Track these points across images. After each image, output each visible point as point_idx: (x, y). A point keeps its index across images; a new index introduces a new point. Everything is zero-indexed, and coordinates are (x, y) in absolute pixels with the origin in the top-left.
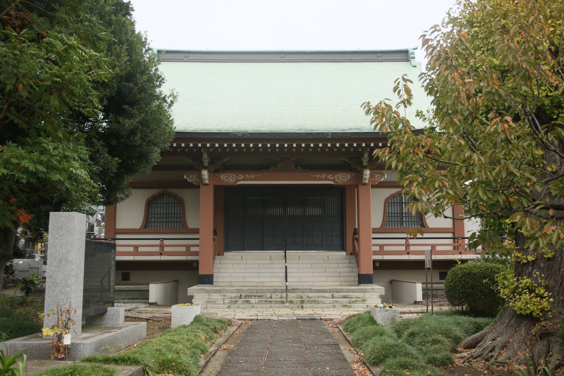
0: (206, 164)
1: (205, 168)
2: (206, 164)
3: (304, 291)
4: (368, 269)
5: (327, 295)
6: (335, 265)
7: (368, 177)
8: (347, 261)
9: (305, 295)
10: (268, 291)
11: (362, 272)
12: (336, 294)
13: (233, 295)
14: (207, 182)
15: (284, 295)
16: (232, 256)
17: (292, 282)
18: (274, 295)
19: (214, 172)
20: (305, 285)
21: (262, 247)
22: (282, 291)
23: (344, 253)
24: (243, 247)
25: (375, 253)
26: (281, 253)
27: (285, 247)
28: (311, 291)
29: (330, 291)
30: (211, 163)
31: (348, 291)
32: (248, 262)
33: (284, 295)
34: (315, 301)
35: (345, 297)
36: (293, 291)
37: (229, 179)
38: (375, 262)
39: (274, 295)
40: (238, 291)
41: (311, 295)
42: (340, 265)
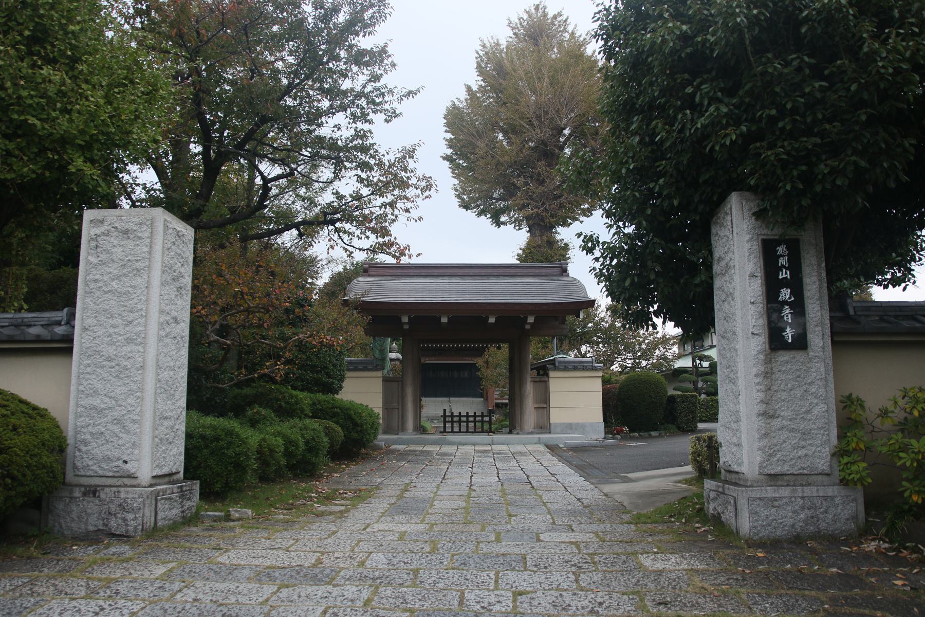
25: (496, 399)
26: (447, 399)
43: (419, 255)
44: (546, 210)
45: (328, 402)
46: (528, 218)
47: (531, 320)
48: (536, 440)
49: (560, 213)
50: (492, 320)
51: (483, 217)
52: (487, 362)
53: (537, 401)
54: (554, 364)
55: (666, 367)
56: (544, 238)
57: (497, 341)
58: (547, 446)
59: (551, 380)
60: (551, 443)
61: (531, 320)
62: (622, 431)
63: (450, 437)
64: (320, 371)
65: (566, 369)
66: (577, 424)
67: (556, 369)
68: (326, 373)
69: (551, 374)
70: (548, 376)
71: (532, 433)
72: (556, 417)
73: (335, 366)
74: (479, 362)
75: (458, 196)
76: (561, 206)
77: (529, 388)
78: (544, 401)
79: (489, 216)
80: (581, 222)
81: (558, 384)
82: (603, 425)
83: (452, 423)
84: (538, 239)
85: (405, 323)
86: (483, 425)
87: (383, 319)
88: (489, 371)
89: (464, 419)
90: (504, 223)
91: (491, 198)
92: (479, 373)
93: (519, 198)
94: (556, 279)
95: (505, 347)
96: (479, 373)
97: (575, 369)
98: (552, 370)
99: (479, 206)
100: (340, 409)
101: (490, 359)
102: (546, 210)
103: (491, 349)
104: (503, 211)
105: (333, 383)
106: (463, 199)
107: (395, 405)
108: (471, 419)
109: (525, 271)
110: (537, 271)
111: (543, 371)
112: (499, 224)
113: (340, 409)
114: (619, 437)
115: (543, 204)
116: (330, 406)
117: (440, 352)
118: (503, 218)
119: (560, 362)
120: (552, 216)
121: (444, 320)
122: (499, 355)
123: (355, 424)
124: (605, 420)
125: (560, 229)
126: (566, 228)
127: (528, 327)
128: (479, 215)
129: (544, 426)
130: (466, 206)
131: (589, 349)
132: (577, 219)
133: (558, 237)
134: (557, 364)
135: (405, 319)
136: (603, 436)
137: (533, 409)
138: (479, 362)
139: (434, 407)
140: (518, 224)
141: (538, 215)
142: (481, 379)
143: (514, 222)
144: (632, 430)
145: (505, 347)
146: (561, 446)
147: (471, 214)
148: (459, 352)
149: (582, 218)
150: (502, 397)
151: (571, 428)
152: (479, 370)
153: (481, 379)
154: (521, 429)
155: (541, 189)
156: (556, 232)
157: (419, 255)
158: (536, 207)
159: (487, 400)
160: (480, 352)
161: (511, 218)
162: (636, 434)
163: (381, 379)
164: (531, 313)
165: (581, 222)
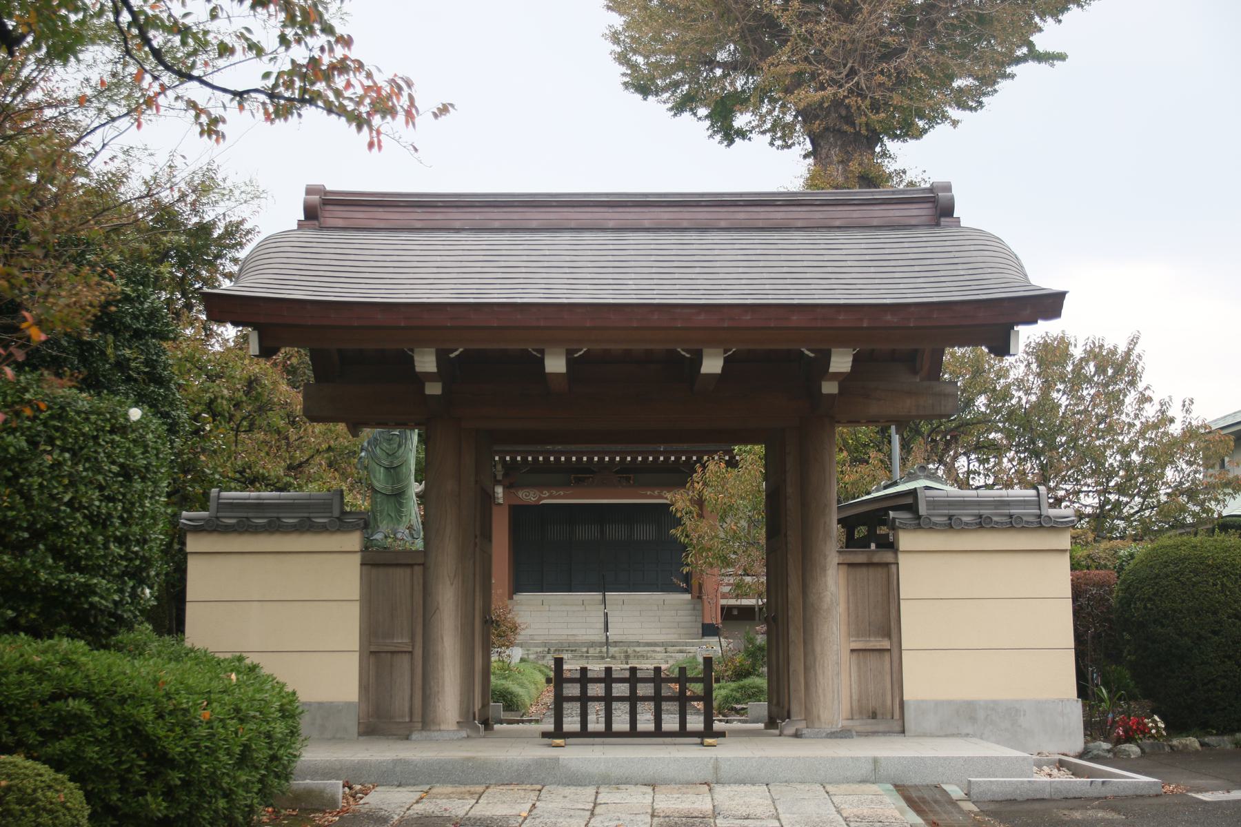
0: (499, 477)
1: (498, 482)
2: (499, 477)
3: (630, 644)
4: (715, 618)
5: (658, 649)
6: (673, 613)
7: (501, 495)
8: (690, 607)
9: (630, 650)
10: (583, 644)
11: (707, 621)
12: (670, 649)
13: (539, 650)
14: (501, 501)
15: (604, 649)
16: (522, 597)
17: (613, 634)
18: (591, 650)
19: (508, 487)
20: (632, 638)
21: (568, 585)
22: (601, 645)
23: (688, 596)
24: (541, 587)
25: (724, 596)
26: (597, 596)
27: (602, 584)
28: (638, 644)
29: (662, 644)
30: (506, 475)
31: (686, 644)
32: (552, 608)
33: (604, 649)
34: (643, 656)
35: (681, 652)
36: (616, 644)
37: (529, 496)
38: (723, 608)
39: (591, 650)
40: (545, 644)
41: (638, 649)
42: (680, 613)
43: (444, 110)
44: (857, 91)
45: (40, 673)
46: (807, 114)
47: (841, 362)
48: (866, 769)
49: (896, 99)
50: (712, 365)
51: (687, 115)
52: (700, 502)
53: (859, 628)
54: (912, 508)
55: (1194, 515)
56: (854, 166)
57: (724, 438)
58: (896, 786)
59: (902, 559)
60: (914, 779)
61: (841, 362)
62: (1144, 731)
63: (575, 755)
64: (31, 543)
65: (952, 525)
66: (993, 706)
67: (919, 523)
68: (57, 553)
69: (906, 540)
70: (892, 546)
71: (843, 734)
72: (923, 680)
73: (99, 522)
74: (679, 500)
75: (622, 59)
76: (901, 80)
77: (834, 587)
78: (882, 624)
79: (703, 112)
80: (955, 123)
81: (928, 573)
82: (1076, 710)
83: (587, 699)
84: (836, 171)
85: (429, 376)
86: (685, 702)
87: (355, 358)
88: (704, 526)
89: (621, 689)
90: (742, 134)
91: (711, 63)
92: (676, 532)
93: (784, 60)
94: (923, 234)
95: (752, 456)
96: (676, 532)
97: (983, 524)
98: (905, 528)
99: (676, 85)
100: (89, 697)
101: (708, 493)
102: (857, 91)
103: (711, 466)
104: (738, 101)
105: (90, 590)
106: (634, 67)
107: (402, 641)
108: (645, 690)
109: (818, 215)
110: (857, 214)
111: (873, 531)
112: (730, 135)
113: (89, 697)
114: (1133, 749)
115: (853, 72)
116: (47, 688)
117: (579, 475)
118: (742, 120)
119: (933, 504)
120: (875, 107)
121: (555, 364)
122: (729, 489)
123: (160, 761)
124: (1082, 692)
125: (892, 146)
126: (912, 143)
127: (830, 388)
128: (679, 108)
129: (884, 713)
130: (643, 86)
131: (975, 465)
132: (945, 117)
133: (890, 166)
134: (923, 510)
135: (426, 362)
136: (1078, 743)
137: (845, 655)
138: (679, 500)
139: (555, 622)
140: (782, 134)
141: (837, 103)
142: (684, 547)
143: (773, 129)
144: (1176, 726)
145: (752, 456)
146: (955, 792)
147: (656, 108)
148: (628, 475)
149: (954, 113)
150: (739, 590)
151: (973, 719)
152: (678, 522)
153: (684, 547)
154: (809, 718)
155: (846, 30)
156: (884, 154)
157: (444, 110)
158: (833, 82)
159: (700, 597)
160: (679, 475)
161: (762, 119)
162: (1193, 742)
163: (357, 559)
164: (843, 338)
165: (955, 123)
